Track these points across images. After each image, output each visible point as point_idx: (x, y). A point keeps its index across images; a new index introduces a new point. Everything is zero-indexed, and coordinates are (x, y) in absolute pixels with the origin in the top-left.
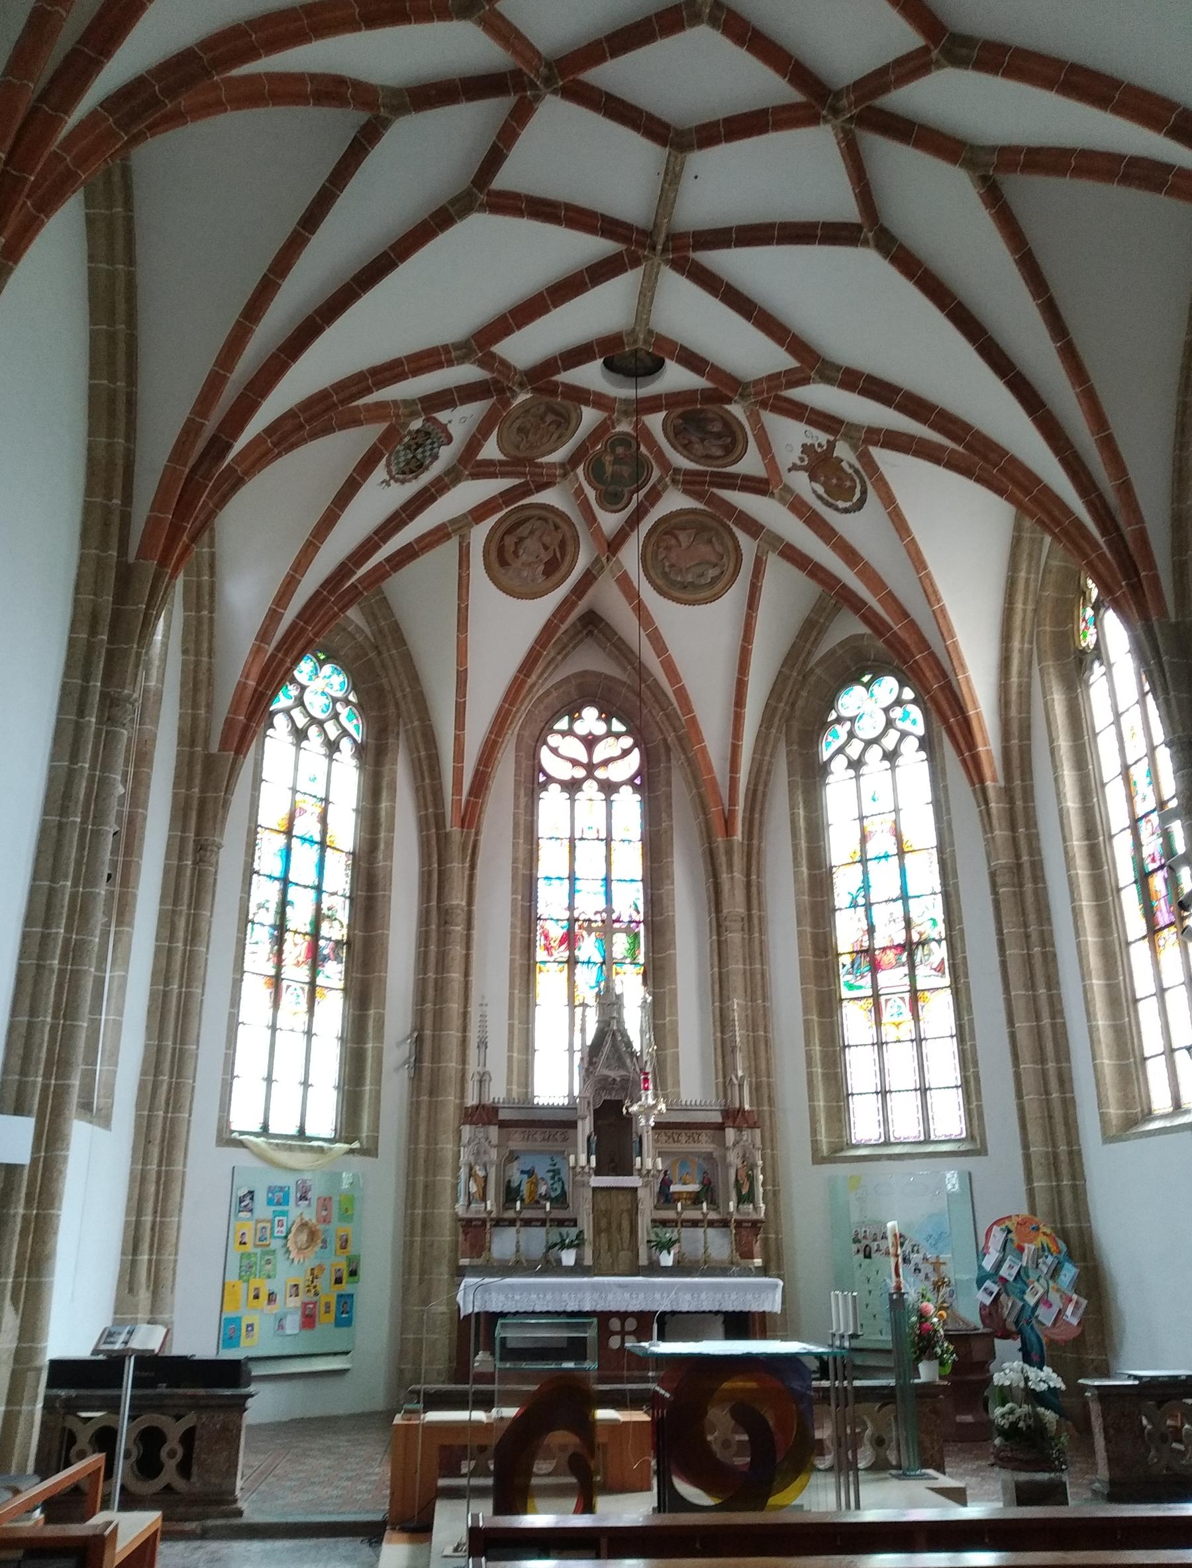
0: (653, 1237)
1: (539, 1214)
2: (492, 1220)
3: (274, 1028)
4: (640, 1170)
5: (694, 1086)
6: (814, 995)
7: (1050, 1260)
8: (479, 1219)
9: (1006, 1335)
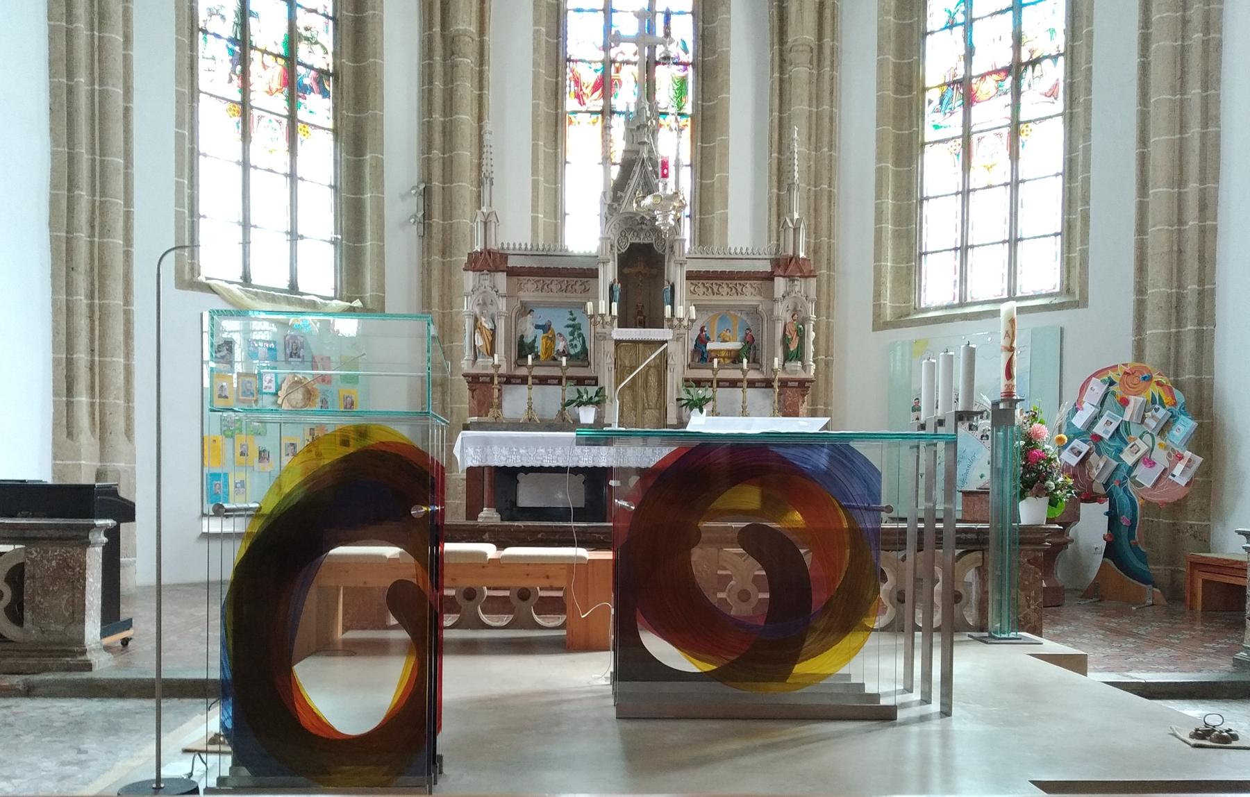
0: (684, 395)
1: (555, 372)
2: (499, 376)
3: (246, 165)
4: (670, 320)
5: (743, 233)
6: (891, 139)
7: (1162, 412)
8: (487, 375)
9: (1091, 498)
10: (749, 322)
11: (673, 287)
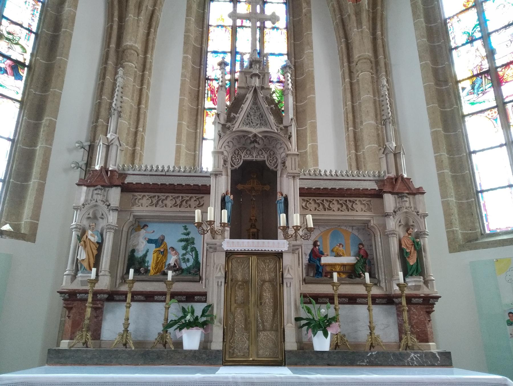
0: (303, 314)
2: (96, 293)
4: (286, 228)
10: (360, 237)
11: (286, 199)
